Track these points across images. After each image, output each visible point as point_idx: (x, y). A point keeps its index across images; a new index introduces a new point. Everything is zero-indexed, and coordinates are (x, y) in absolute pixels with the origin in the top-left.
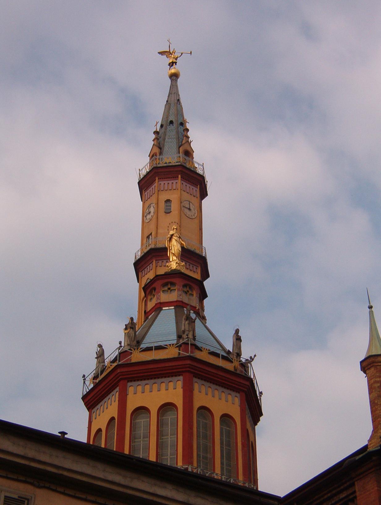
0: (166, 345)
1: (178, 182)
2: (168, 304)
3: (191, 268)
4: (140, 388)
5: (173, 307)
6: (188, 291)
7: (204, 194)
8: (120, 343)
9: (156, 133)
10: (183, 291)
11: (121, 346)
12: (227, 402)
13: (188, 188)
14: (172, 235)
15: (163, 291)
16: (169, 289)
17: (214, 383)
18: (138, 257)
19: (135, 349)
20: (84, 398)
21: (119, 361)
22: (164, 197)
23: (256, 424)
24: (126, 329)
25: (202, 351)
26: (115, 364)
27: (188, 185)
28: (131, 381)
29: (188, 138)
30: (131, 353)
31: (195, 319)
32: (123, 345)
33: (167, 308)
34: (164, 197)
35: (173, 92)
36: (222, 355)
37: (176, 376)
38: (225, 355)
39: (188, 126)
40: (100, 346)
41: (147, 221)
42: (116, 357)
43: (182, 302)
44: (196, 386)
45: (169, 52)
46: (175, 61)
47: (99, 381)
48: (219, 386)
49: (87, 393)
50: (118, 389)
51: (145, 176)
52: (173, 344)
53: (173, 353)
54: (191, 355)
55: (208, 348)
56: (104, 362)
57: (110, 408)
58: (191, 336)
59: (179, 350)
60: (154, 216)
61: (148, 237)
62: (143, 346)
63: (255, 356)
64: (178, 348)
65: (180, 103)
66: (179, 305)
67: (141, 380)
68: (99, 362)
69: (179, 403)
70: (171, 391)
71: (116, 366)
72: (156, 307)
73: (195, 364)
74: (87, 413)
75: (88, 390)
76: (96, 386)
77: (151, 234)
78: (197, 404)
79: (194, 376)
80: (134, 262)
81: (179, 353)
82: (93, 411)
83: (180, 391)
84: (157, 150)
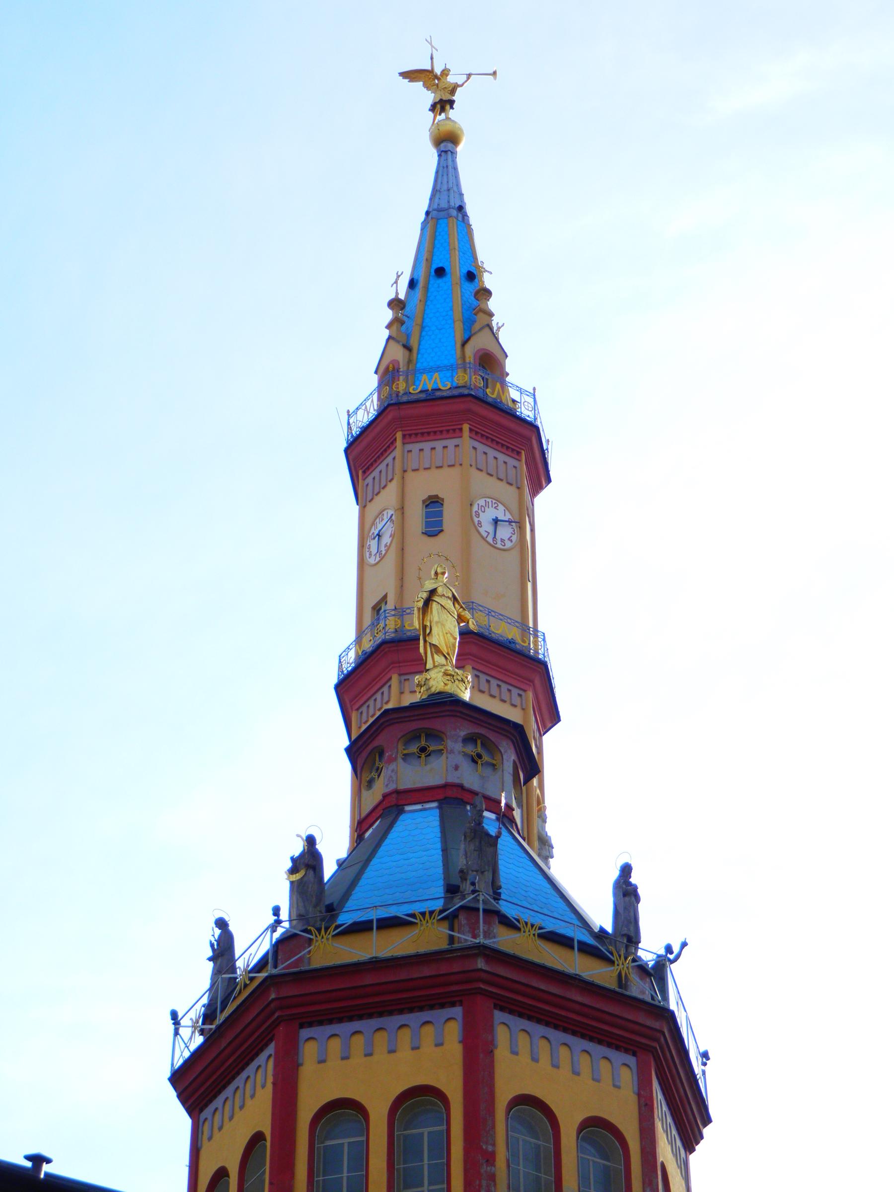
0: (413, 915)
1: (466, 444)
2: (420, 795)
3: (494, 691)
4: (335, 1045)
5: (435, 804)
6: (480, 756)
7: (539, 476)
8: (276, 911)
9: (396, 304)
10: (465, 755)
11: (278, 922)
12: (598, 1081)
13: (500, 462)
14: (433, 592)
15: (406, 757)
16: (423, 750)
17: (556, 1027)
18: (348, 667)
19: (319, 930)
20: (178, 1078)
21: (275, 967)
22: (422, 485)
23: (690, 1148)
24: (293, 871)
25: (519, 929)
26: (263, 975)
27: (492, 453)
28: (311, 1025)
29: (491, 315)
30: (311, 940)
31: (498, 837)
32: (284, 915)
33: (419, 807)
34: (422, 485)
35: (445, 187)
36: (579, 942)
37: (442, 1006)
38: (591, 941)
39: (488, 281)
40: (222, 924)
41: (372, 561)
42: (267, 954)
43: (461, 787)
44: (502, 1035)
45: (431, 71)
46: (446, 97)
47: (219, 1027)
48: (574, 1033)
49: (186, 1062)
50: (271, 1049)
51: (365, 430)
52: (431, 913)
53: (430, 938)
54: (487, 942)
55: (538, 920)
56: (233, 969)
57: (251, 1108)
58: (483, 885)
59: (452, 928)
60: (393, 548)
61: (377, 609)
62: (345, 918)
63: (684, 945)
64: (446, 924)
65: (465, 216)
66: (451, 798)
67: (341, 1020)
68: (217, 973)
69: (453, 1086)
70: (427, 1052)
71: (266, 978)
72: (385, 804)
73: (502, 971)
74: (183, 1122)
75: (187, 1054)
76: (211, 1040)
77: (385, 596)
78: (506, 1089)
79: (496, 1007)
80: (335, 681)
81: (451, 939)
82: (203, 1116)
83: (454, 1048)
84: (399, 354)
